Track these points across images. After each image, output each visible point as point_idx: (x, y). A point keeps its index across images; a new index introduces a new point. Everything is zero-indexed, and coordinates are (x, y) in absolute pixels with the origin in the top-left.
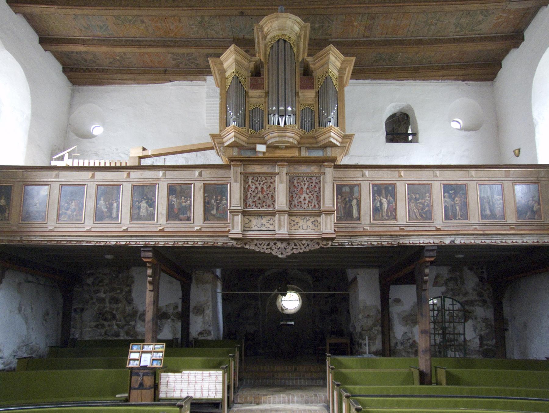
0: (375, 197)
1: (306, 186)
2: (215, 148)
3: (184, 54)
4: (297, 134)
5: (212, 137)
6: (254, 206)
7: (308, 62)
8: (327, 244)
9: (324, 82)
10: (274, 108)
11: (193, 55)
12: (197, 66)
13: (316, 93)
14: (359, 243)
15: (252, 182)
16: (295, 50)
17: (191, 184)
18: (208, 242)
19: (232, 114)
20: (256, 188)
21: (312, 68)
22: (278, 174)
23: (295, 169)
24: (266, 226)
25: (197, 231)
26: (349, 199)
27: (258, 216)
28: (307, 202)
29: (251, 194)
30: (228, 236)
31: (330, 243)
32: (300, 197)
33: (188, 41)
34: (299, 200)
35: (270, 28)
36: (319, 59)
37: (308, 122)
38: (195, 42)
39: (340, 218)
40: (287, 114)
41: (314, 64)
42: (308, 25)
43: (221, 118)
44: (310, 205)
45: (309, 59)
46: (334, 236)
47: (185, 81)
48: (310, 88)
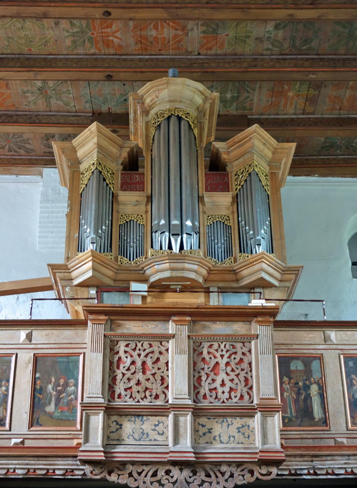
0: (351, 380)
1: (225, 360)
2: (55, 287)
3: (8, 134)
4: (201, 264)
5: (52, 269)
6: (128, 396)
7: (218, 150)
8: (269, 474)
9: (246, 180)
10: (163, 222)
11: (24, 136)
12: (28, 152)
13: (233, 198)
14: (330, 471)
15: (126, 352)
16: (196, 131)
17: (11, 355)
18: (35, 470)
19: (88, 230)
20: (133, 363)
21: (225, 159)
22: (173, 336)
23: (204, 327)
24: (150, 437)
25: (16, 447)
26: (304, 384)
27: (134, 415)
28: (227, 389)
29: (124, 374)
30: (76, 456)
31: (274, 471)
32: (214, 381)
33: (17, 115)
34: (213, 386)
35: (156, 99)
36: (236, 146)
37: (220, 246)
38: (28, 116)
39: (290, 420)
40: (184, 232)
41: (228, 153)
42: (216, 94)
43: (69, 238)
44: (233, 394)
45: (219, 145)
46: (282, 456)
47: (6, 174)
48: (223, 190)
